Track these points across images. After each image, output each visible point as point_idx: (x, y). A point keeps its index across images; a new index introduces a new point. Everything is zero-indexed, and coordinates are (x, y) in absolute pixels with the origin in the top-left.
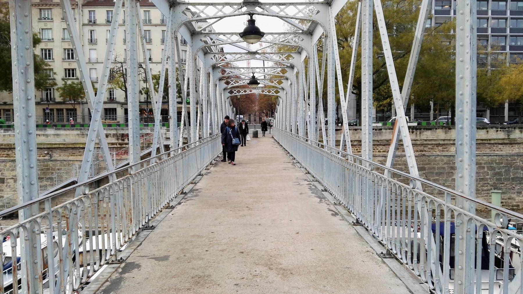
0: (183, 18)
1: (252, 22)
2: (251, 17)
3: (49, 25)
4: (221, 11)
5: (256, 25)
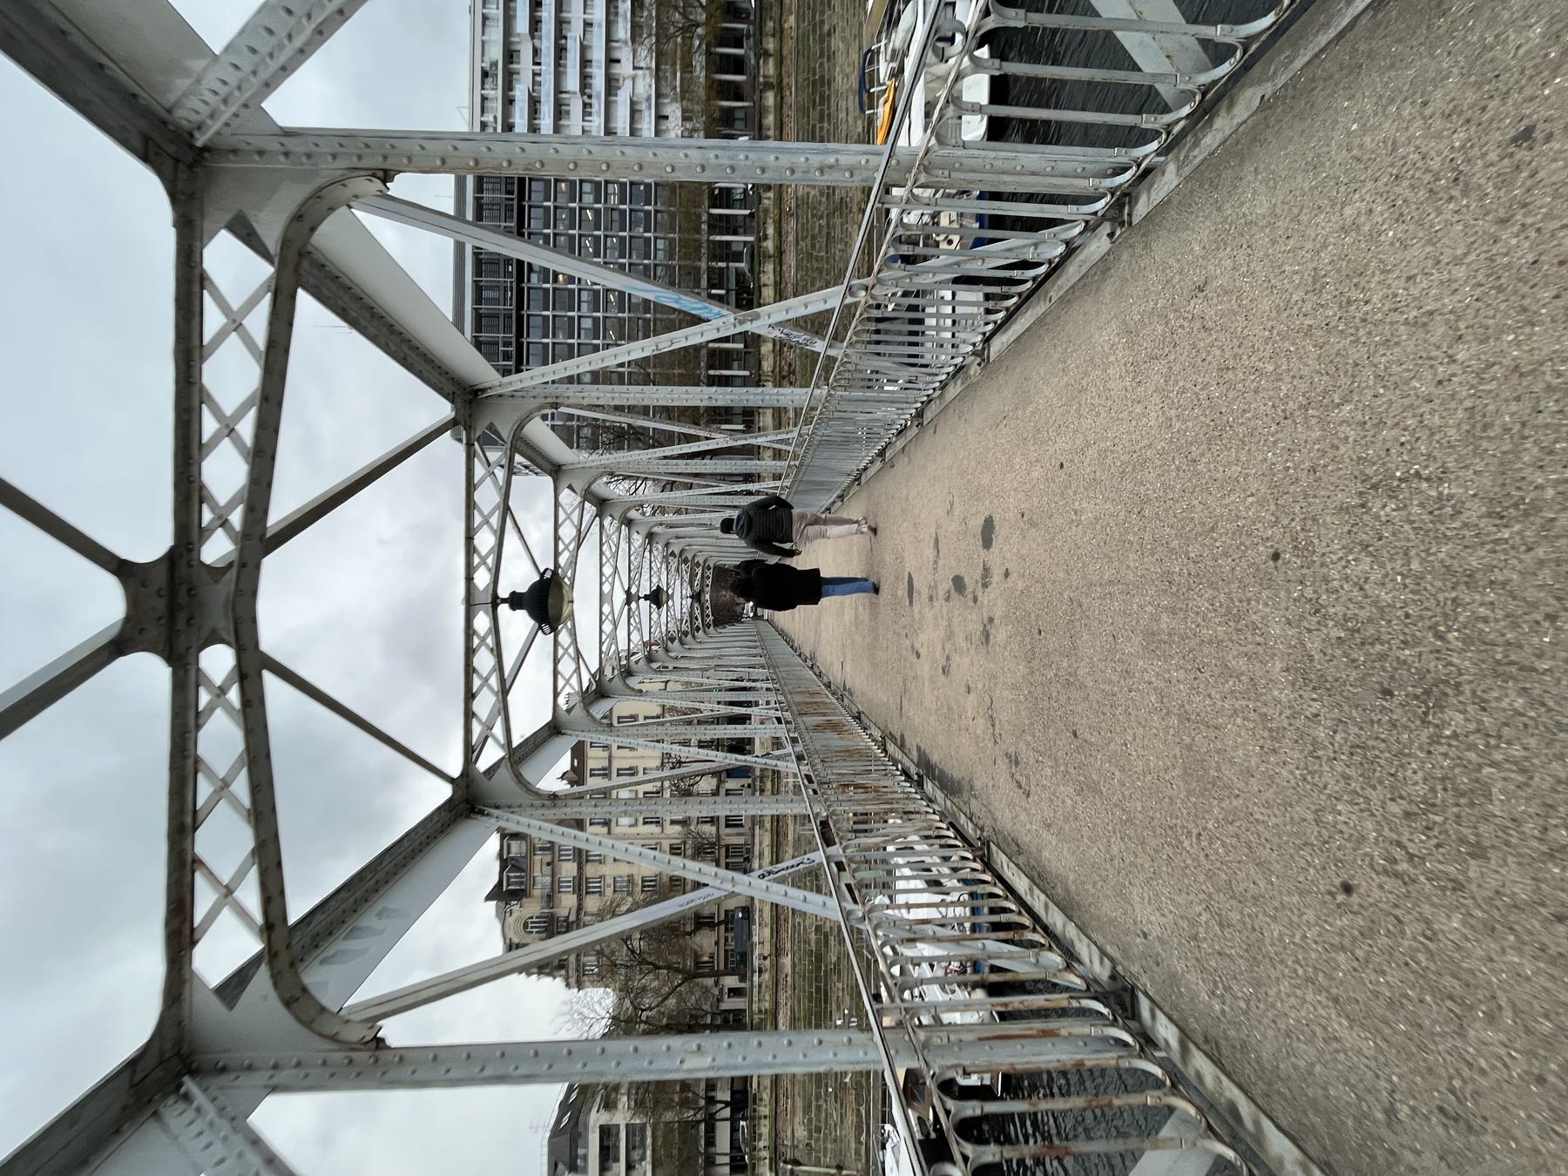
0: (578, 712)
1: (516, 601)
2: (504, 601)
3: (610, 881)
4: (486, 680)
5: (524, 590)
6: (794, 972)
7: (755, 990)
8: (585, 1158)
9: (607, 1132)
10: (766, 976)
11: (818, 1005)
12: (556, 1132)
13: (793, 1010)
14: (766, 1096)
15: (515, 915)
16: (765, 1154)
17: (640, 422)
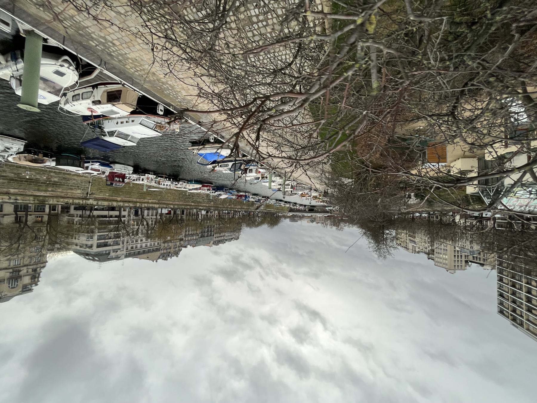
6: (18, 189)
7: (24, 202)
8: (106, 251)
9: (99, 246)
10: (19, 198)
11: (33, 182)
12: (100, 261)
13: (34, 190)
14: (66, 200)
15: (6, 293)
16: (84, 201)
17: (153, 205)
